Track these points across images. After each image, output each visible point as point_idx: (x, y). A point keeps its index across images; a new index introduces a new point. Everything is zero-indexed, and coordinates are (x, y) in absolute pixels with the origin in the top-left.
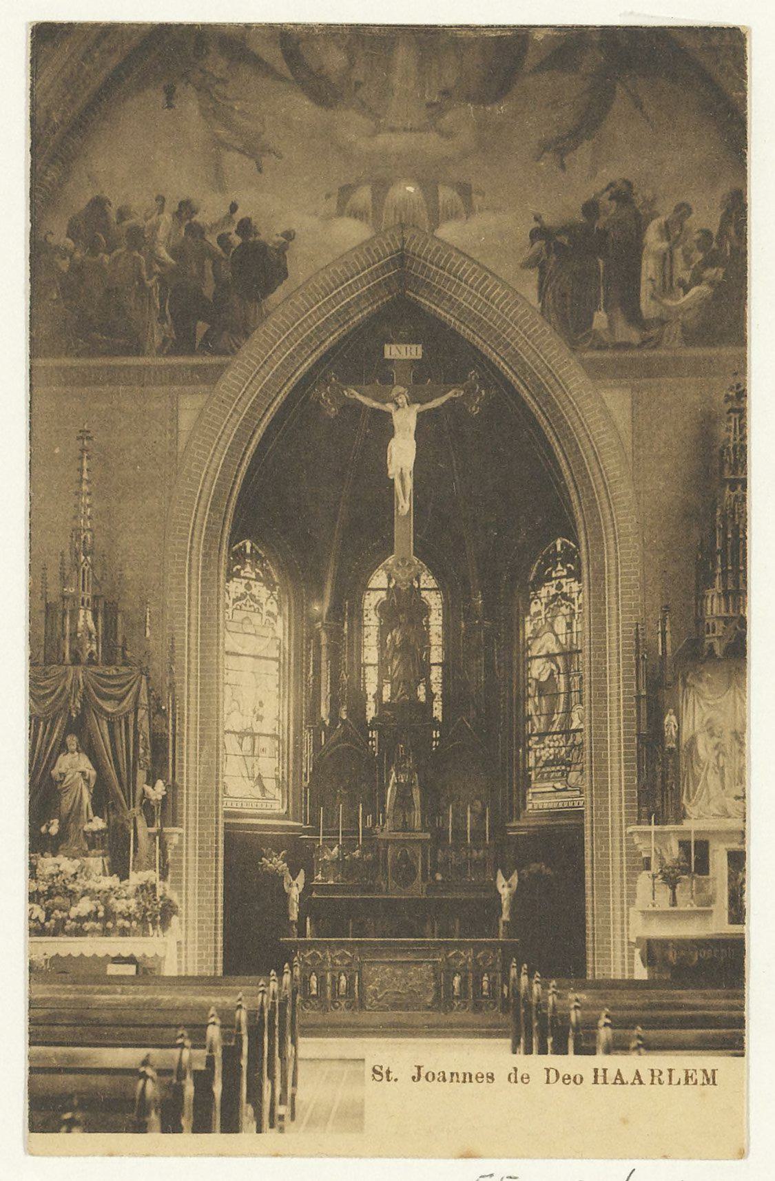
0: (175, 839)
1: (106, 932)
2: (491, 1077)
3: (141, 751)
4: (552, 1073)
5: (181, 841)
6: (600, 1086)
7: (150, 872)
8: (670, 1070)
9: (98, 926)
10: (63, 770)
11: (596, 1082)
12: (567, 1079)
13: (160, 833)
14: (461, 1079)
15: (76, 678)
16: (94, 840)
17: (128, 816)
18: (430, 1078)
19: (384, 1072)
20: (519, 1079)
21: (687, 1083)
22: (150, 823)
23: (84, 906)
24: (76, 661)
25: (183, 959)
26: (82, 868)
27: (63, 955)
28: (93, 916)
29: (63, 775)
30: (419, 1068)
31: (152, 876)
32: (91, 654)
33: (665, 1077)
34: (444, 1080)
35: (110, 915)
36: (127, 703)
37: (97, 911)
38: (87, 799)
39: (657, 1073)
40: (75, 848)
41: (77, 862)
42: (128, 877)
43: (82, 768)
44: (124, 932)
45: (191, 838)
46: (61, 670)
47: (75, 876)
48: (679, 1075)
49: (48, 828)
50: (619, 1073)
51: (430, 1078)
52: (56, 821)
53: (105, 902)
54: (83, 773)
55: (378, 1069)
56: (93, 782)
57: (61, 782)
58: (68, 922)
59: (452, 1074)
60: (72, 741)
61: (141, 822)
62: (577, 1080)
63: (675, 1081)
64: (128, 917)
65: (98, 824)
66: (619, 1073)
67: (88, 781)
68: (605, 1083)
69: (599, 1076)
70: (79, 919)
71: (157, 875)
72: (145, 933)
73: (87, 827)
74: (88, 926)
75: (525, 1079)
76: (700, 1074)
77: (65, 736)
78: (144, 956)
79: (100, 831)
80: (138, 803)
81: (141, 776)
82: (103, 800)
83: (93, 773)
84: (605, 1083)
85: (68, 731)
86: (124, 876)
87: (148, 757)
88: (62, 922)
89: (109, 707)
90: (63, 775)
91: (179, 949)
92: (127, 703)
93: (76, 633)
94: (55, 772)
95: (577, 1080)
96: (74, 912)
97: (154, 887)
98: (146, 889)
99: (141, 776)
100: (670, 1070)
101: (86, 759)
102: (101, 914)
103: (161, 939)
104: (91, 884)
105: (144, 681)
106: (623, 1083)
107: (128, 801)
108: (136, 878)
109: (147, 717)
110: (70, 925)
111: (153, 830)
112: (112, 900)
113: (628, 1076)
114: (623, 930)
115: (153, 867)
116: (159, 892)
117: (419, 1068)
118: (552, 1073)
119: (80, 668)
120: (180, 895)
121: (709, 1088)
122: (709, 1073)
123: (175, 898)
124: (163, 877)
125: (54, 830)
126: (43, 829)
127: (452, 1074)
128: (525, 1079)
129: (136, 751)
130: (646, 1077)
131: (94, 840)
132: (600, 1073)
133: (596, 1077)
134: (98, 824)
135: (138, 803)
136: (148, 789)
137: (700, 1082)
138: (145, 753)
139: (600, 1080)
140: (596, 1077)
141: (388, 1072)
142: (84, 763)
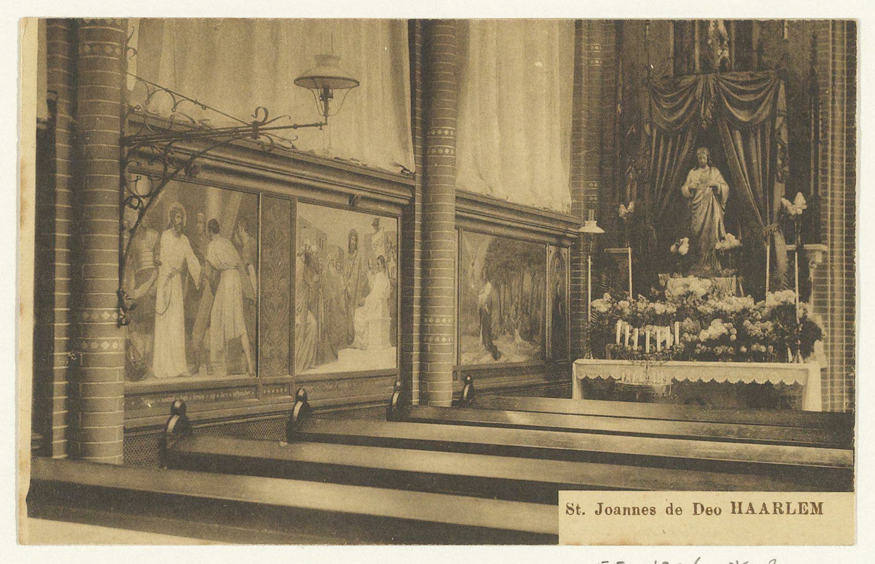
0: (819, 258)
1: (739, 357)
2: (653, 511)
3: (779, 162)
4: (699, 507)
5: (825, 260)
6: (737, 515)
7: (790, 292)
8: (788, 503)
9: (730, 350)
10: (693, 186)
11: (734, 512)
12: (709, 512)
13: (800, 249)
14: (631, 512)
15: (706, 86)
16: (726, 258)
17: (766, 230)
18: (609, 511)
19: (574, 507)
20: (674, 512)
21: (801, 513)
22: (789, 241)
23: (717, 329)
24: (707, 66)
25: (829, 387)
26: (714, 288)
27: (706, 381)
28: (723, 339)
29: (693, 191)
30: (600, 504)
31: (790, 296)
32: (724, 61)
33: (784, 509)
34: (619, 513)
35: (745, 337)
36: (764, 112)
37: (730, 334)
38: (718, 216)
39: (778, 505)
40: (708, 268)
41: (708, 282)
42: (764, 298)
43: (713, 182)
44: (758, 357)
45: (836, 257)
46: (690, 79)
47: (705, 297)
48: (794, 506)
49: (678, 247)
50: (750, 505)
51: (609, 511)
52: (686, 240)
53: (739, 325)
54: (715, 188)
55: (570, 505)
56: (725, 197)
57: (692, 198)
58: (699, 345)
59: (625, 509)
60: (703, 154)
61: (779, 240)
62: (717, 512)
63: (791, 511)
64: (765, 341)
65: (731, 241)
66: (750, 505)
67: (719, 197)
68: (740, 512)
69: (736, 508)
70: (710, 342)
71: (797, 295)
72: (783, 359)
73: (718, 246)
74: (720, 350)
75: (679, 511)
76: (810, 506)
77: (695, 150)
78: (782, 383)
79: (732, 250)
80: (775, 218)
81: (779, 189)
82: (737, 215)
83: (725, 188)
84: (740, 512)
85: (699, 144)
86: (759, 297)
87: (786, 169)
88: (692, 345)
89: (742, 116)
90: (693, 191)
91: (824, 377)
92: (764, 112)
93: (707, 38)
94: (685, 189)
95: (717, 512)
96: (704, 335)
97: (793, 308)
98: (786, 310)
99: (779, 189)
100: (788, 503)
101: (718, 172)
102: (734, 337)
103: (802, 365)
104: (722, 305)
105: (782, 87)
106: (753, 513)
107: (764, 219)
108: (772, 299)
109: (785, 125)
110: (700, 349)
111: (793, 247)
112: (747, 322)
113: (758, 508)
114: (832, 398)
115: (792, 286)
116: (800, 313)
117: (600, 504)
118: (699, 507)
119: (711, 76)
120: (825, 318)
121: (817, 516)
122: (817, 505)
123: (819, 321)
124: (804, 298)
125: (684, 249)
126: (673, 248)
127: (634, 509)
128: (679, 511)
129: (773, 160)
130: (770, 508)
131: (726, 258)
132: (737, 505)
133: (734, 507)
134: (731, 241)
135: (775, 218)
136: (786, 202)
137: (810, 512)
138: (783, 165)
139: (737, 510)
140: (734, 507)
141: (578, 508)
142: (716, 177)
